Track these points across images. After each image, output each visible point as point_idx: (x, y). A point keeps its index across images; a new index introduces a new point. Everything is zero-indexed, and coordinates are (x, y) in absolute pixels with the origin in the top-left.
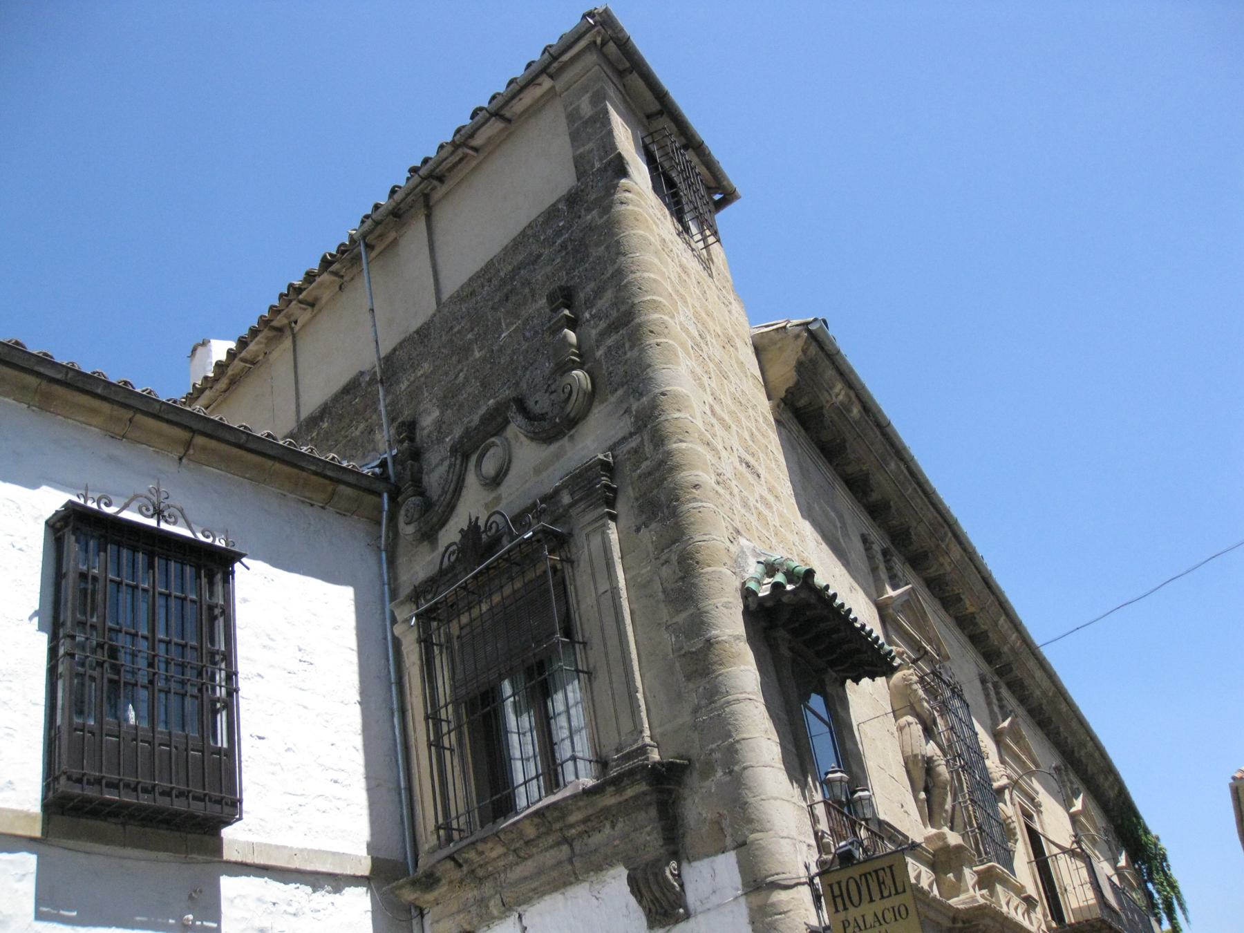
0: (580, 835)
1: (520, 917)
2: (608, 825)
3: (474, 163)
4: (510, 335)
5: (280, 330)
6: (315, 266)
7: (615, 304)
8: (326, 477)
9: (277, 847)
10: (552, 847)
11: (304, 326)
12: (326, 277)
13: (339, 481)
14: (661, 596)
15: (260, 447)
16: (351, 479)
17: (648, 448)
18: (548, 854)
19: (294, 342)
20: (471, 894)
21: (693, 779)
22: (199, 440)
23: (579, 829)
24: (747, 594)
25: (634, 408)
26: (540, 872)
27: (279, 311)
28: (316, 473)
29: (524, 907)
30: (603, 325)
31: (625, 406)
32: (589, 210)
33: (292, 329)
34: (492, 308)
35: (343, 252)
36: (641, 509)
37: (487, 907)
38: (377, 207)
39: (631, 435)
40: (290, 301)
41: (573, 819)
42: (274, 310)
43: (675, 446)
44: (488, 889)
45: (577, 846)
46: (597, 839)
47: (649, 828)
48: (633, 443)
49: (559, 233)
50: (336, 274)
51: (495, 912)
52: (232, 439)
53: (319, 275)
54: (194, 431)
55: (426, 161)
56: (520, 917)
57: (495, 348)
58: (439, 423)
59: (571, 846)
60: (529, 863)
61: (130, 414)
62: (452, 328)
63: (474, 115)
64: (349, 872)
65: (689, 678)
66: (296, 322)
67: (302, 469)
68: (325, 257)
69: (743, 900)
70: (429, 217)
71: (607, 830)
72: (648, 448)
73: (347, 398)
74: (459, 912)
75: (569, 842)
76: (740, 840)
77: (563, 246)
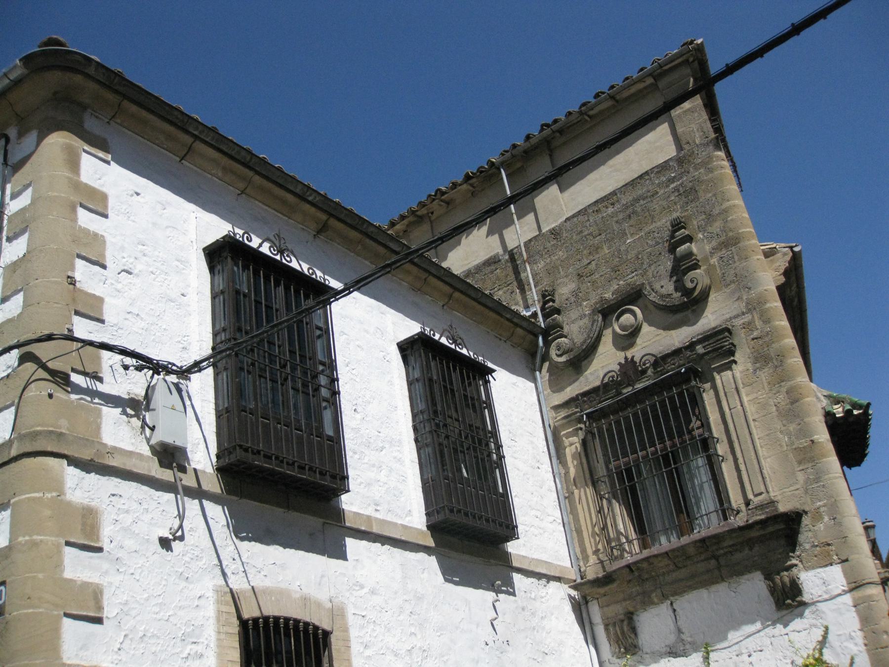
0: (725, 554)
1: (672, 604)
2: (747, 549)
3: (588, 126)
4: (634, 241)
5: (421, 218)
6: (460, 180)
7: (724, 230)
8: (512, 322)
9: (524, 557)
10: (702, 561)
11: (438, 218)
12: (465, 186)
13: (517, 325)
14: (776, 414)
15: (483, 300)
16: (525, 324)
17: (758, 323)
18: (699, 565)
19: (432, 226)
20: (636, 589)
21: (806, 520)
22: (457, 295)
23: (726, 550)
24: (829, 416)
25: (745, 297)
26: (693, 576)
27: (424, 206)
28: (508, 319)
29: (676, 597)
30: (714, 243)
31: (737, 295)
32: (696, 169)
33: (430, 217)
34: (617, 222)
35: (481, 172)
36: (756, 360)
37: (650, 597)
38: (514, 146)
39: (743, 314)
40: (434, 200)
41: (725, 544)
42: (422, 205)
43: (777, 323)
44: (648, 586)
45: (722, 561)
46: (738, 556)
47: (781, 550)
48: (747, 318)
49: (672, 180)
50: (472, 185)
51: (656, 600)
52: (473, 295)
53: (460, 185)
54: (456, 289)
55: (556, 121)
56: (672, 604)
57: (623, 248)
58: (575, 293)
59: (717, 560)
60: (683, 570)
61: (424, 275)
62: (581, 232)
63: (597, 96)
64: (552, 574)
65: (800, 463)
66: (432, 213)
67: (501, 316)
68: (467, 173)
69: (104, 616)
70: (551, 156)
71: (746, 551)
72: (758, 323)
73: (489, 269)
74: (625, 600)
75: (716, 558)
76: (844, 558)
77: (676, 189)
